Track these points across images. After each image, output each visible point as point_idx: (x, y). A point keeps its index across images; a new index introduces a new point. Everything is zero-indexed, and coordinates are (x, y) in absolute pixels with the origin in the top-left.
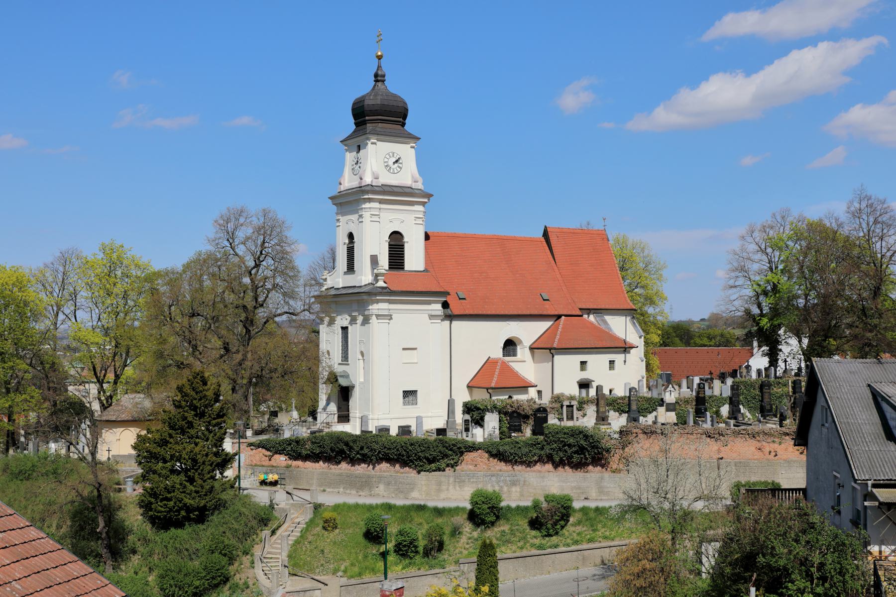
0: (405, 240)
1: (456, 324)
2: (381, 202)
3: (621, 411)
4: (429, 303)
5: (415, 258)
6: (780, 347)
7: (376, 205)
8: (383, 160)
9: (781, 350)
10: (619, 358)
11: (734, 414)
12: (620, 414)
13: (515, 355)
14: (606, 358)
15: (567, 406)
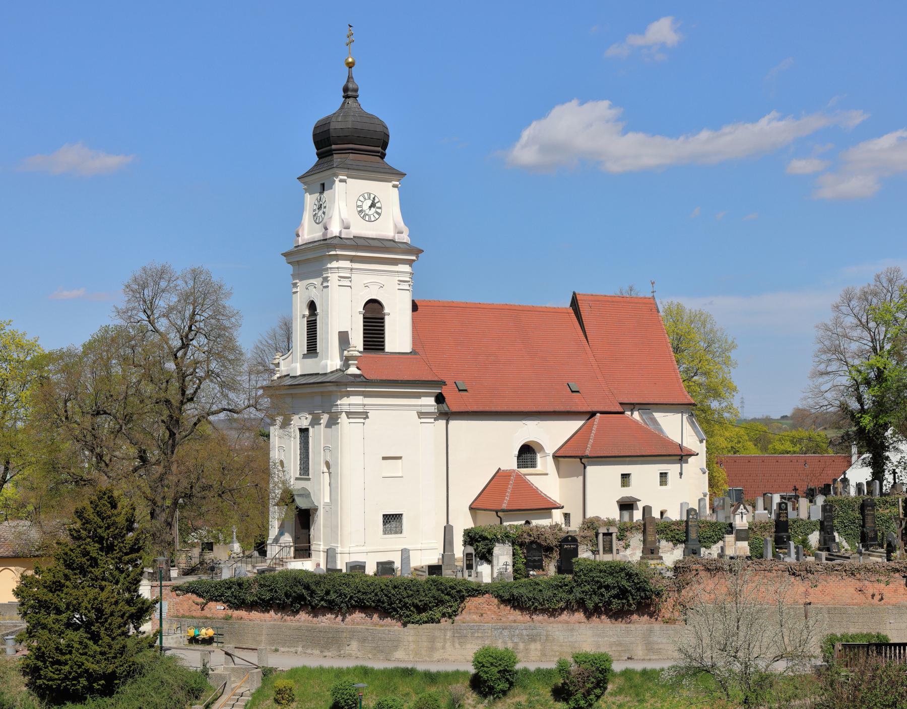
0: (386, 311)
1: (453, 424)
2: (352, 259)
3: (676, 541)
5: (399, 336)
7: (346, 264)
8: (356, 204)
10: (673, 469)
11: (826, 544)
12: (675, 545)
14: (653, 470)
15: (604, 534)
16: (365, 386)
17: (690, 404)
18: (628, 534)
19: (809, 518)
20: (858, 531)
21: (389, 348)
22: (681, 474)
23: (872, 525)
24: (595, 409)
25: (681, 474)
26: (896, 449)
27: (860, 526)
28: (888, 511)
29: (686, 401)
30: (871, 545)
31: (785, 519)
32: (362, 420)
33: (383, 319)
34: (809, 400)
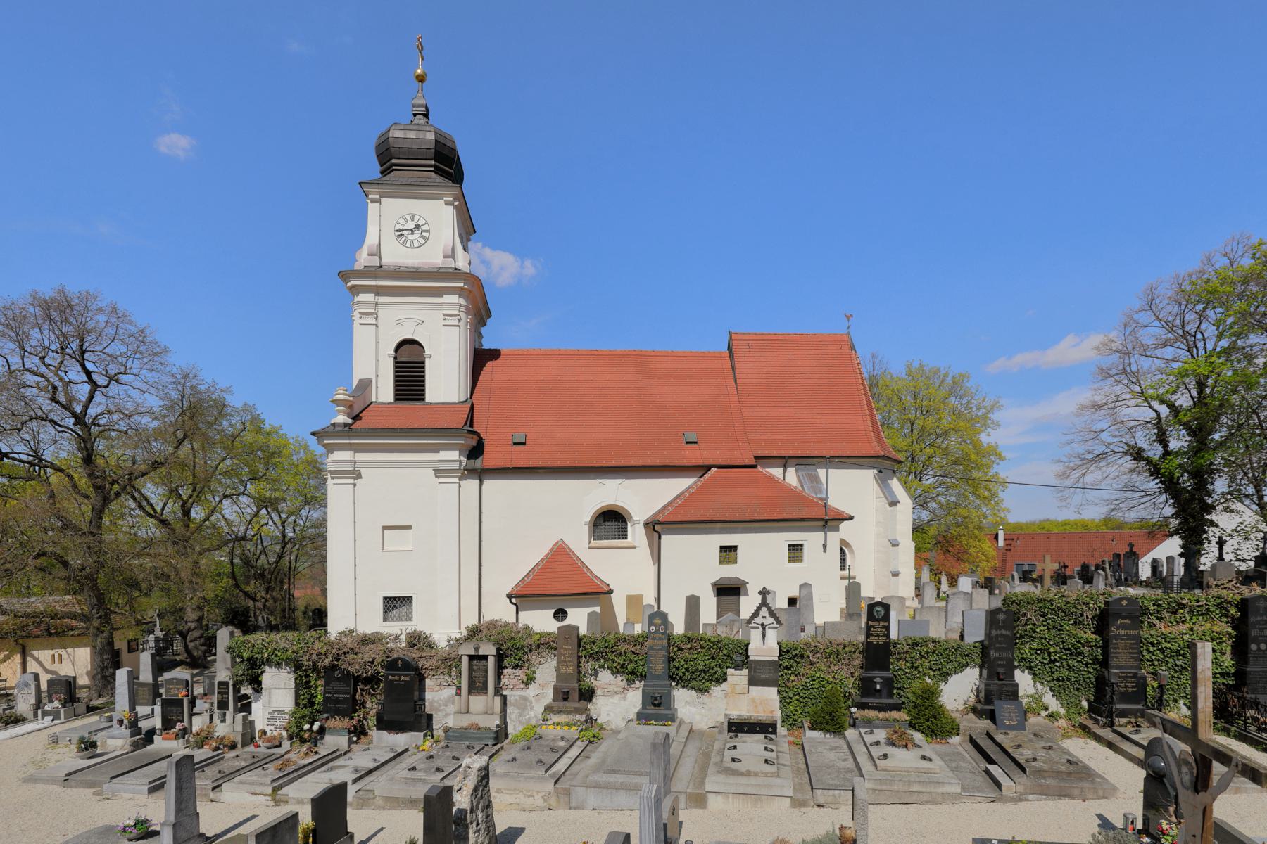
0: (427, 352)
1: (489, 484)
2: (379, 291)
3: (633, 675)
4: (435, 449)
5: (446, 382)
6: (1212, 517)
7: (370, 297)
8: (408, 228)
9: (1213, 524)
10: (811, 540)
11: (995, 697)
12: (630, 682)
13: (624, 536)
14: (780, 541)
15: (471, 658)
16: (349, 437)
17: (878, 457)
18: (532, 657)
19: (962, 637)
20: (1090, 674)
21: (430, 396)
22: (825, 546)
23: (1132, 662)
24: (711, 462)
25: (825, 546)
26: (1228, 510)
27: (1095, 661)
28: (1183, 628)
29: (872, 453)
30: (1123, 714)
31: (882, 640)
32: (352, 481)
33: (423, 362)
34: (1074, 445)
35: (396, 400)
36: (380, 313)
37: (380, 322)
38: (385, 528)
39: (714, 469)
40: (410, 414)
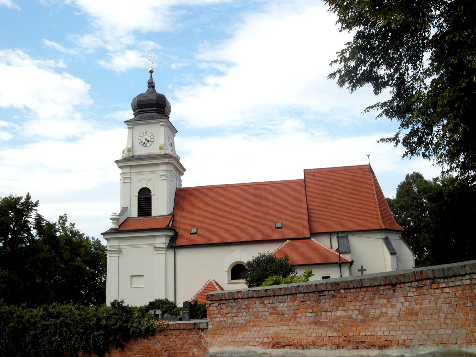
0: (152, 193)
2: (131, 167)
5: (161, 206)
21: (153, 214)
29: (378, 227)
33: (151, 198)
35: (139, 216)
36: (132, 177)
37: (132, 182)
38: (132, 276)
39: (288, 241)
40: (145, 222)
